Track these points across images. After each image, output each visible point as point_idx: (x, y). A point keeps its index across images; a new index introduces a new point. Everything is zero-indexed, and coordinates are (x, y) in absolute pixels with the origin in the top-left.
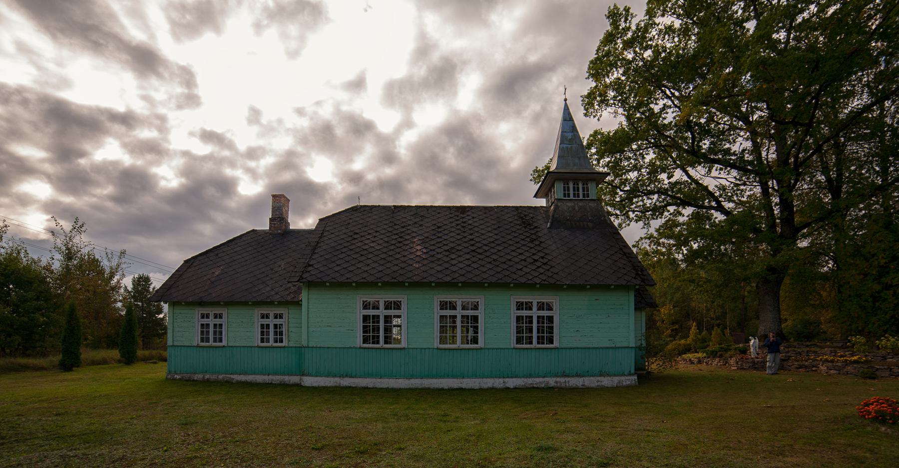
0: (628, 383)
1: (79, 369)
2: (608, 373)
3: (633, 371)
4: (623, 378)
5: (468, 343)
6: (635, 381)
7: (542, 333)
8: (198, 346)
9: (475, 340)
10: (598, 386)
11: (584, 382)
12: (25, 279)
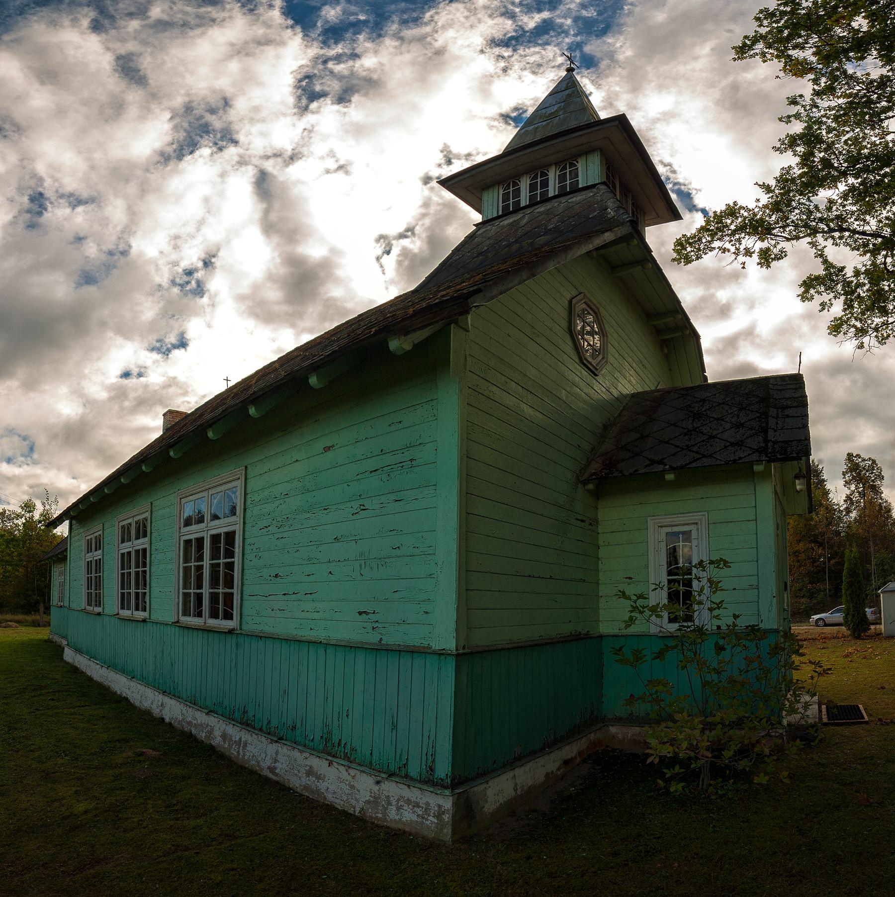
0: (409, 816)
1: (11, 32)
2: (348, 750)
3: (443, 769)
4: (392, 789)
5: (200, 615)
6: (439, 816)
7: (96, 593)
8: (84, 611)
9: (141, 603)
10: (306, 788)
11: (276, 761)
12: (140, 16)
